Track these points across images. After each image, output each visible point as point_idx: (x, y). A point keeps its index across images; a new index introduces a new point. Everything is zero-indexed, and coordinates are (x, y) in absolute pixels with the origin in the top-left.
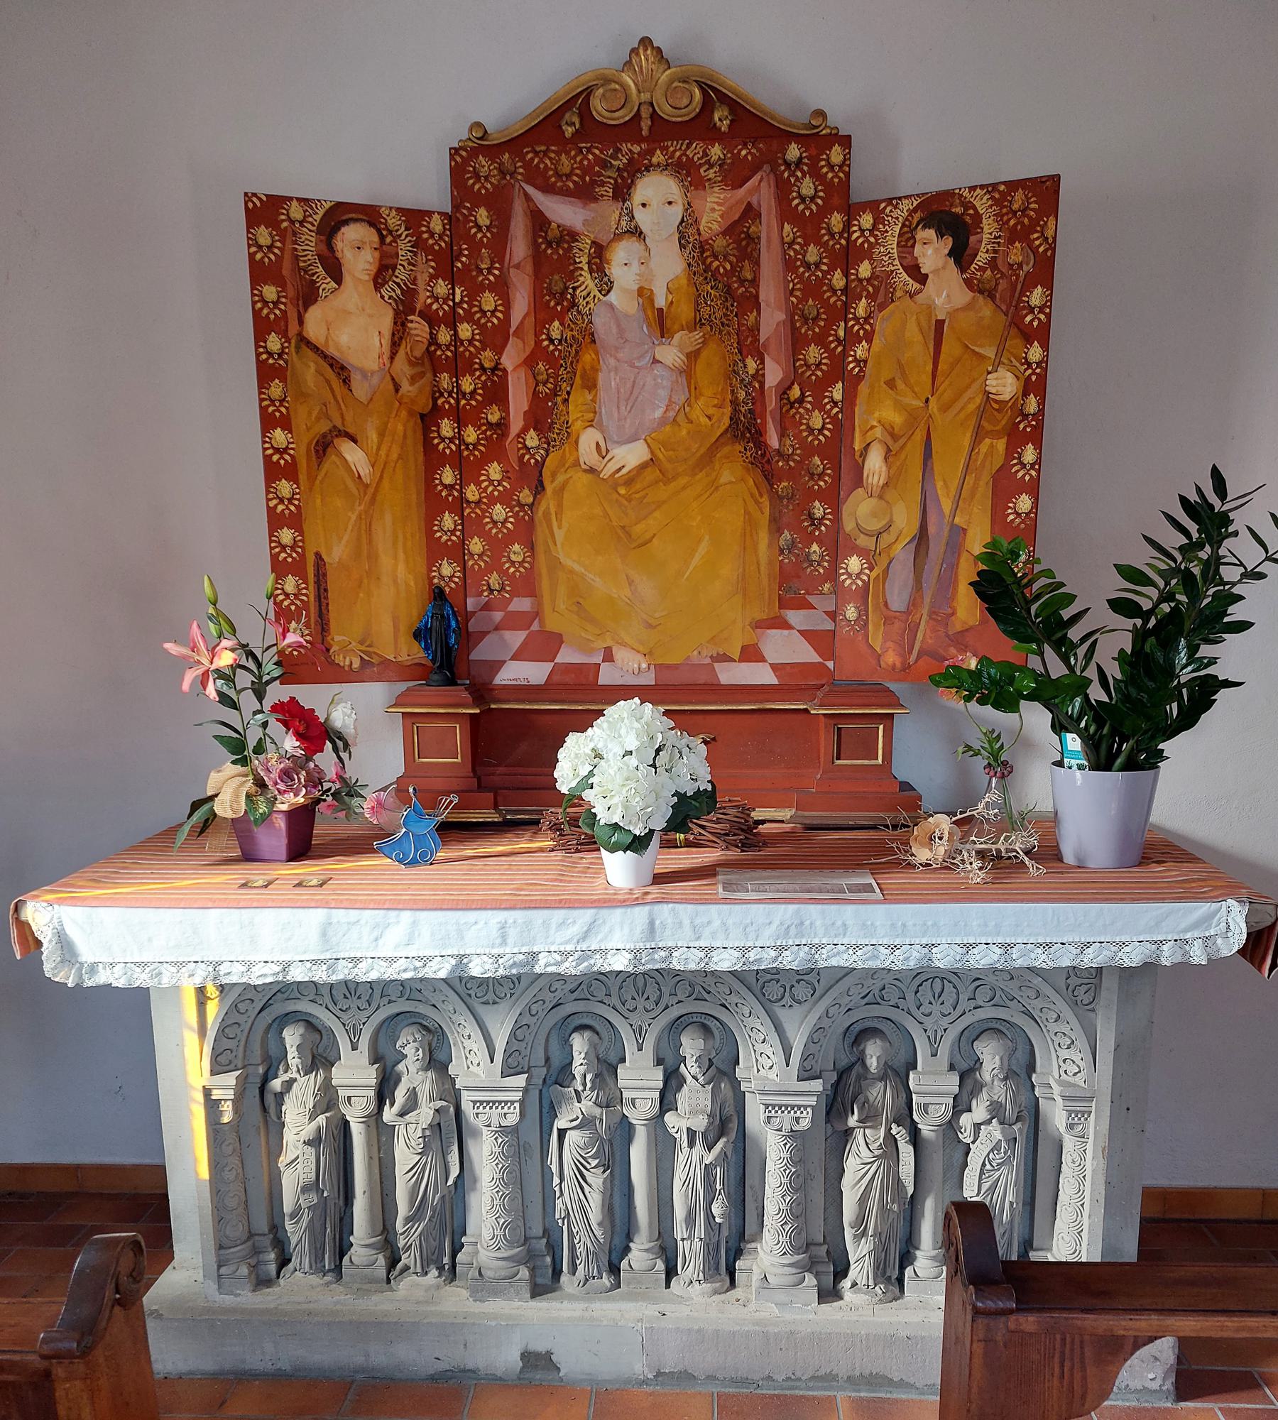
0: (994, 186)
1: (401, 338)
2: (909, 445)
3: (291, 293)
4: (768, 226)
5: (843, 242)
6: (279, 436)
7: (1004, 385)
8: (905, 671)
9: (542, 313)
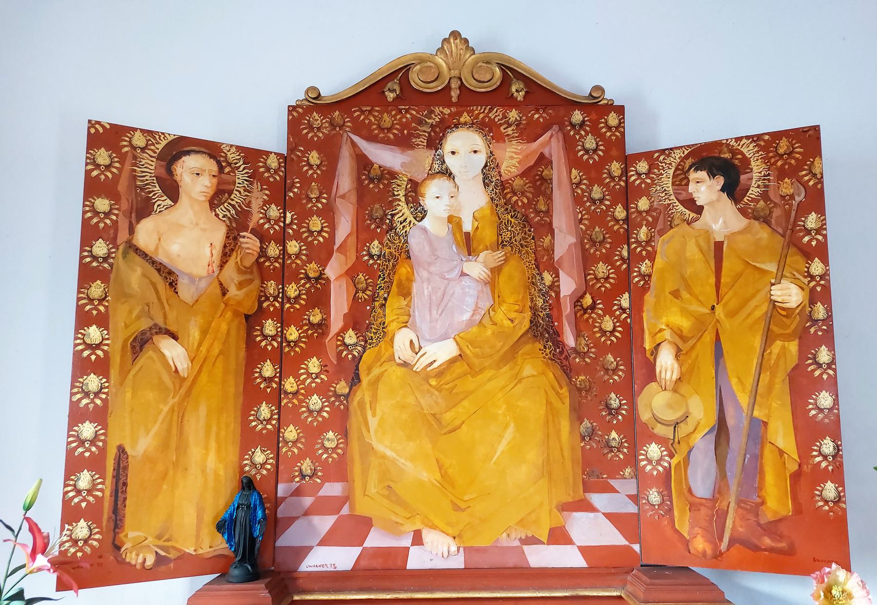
0: (759, 137)
1: (232, 250)
2: (699, 345)
3: (125, 205)
4: (559, 172)
5: (622, 183)
6: (94, 333)
7: (790, 294)
8: (717, 559)
9: (364, 232)
